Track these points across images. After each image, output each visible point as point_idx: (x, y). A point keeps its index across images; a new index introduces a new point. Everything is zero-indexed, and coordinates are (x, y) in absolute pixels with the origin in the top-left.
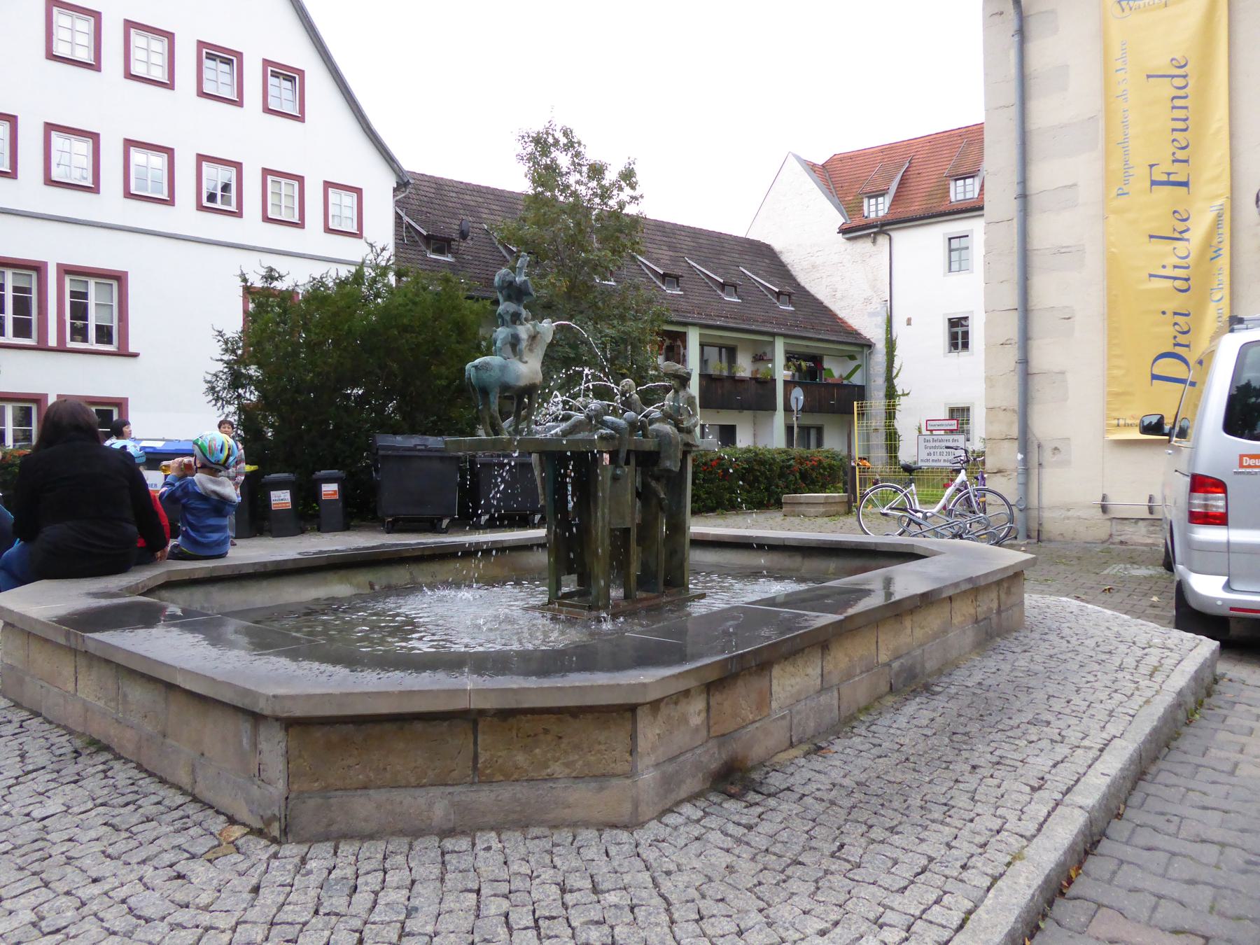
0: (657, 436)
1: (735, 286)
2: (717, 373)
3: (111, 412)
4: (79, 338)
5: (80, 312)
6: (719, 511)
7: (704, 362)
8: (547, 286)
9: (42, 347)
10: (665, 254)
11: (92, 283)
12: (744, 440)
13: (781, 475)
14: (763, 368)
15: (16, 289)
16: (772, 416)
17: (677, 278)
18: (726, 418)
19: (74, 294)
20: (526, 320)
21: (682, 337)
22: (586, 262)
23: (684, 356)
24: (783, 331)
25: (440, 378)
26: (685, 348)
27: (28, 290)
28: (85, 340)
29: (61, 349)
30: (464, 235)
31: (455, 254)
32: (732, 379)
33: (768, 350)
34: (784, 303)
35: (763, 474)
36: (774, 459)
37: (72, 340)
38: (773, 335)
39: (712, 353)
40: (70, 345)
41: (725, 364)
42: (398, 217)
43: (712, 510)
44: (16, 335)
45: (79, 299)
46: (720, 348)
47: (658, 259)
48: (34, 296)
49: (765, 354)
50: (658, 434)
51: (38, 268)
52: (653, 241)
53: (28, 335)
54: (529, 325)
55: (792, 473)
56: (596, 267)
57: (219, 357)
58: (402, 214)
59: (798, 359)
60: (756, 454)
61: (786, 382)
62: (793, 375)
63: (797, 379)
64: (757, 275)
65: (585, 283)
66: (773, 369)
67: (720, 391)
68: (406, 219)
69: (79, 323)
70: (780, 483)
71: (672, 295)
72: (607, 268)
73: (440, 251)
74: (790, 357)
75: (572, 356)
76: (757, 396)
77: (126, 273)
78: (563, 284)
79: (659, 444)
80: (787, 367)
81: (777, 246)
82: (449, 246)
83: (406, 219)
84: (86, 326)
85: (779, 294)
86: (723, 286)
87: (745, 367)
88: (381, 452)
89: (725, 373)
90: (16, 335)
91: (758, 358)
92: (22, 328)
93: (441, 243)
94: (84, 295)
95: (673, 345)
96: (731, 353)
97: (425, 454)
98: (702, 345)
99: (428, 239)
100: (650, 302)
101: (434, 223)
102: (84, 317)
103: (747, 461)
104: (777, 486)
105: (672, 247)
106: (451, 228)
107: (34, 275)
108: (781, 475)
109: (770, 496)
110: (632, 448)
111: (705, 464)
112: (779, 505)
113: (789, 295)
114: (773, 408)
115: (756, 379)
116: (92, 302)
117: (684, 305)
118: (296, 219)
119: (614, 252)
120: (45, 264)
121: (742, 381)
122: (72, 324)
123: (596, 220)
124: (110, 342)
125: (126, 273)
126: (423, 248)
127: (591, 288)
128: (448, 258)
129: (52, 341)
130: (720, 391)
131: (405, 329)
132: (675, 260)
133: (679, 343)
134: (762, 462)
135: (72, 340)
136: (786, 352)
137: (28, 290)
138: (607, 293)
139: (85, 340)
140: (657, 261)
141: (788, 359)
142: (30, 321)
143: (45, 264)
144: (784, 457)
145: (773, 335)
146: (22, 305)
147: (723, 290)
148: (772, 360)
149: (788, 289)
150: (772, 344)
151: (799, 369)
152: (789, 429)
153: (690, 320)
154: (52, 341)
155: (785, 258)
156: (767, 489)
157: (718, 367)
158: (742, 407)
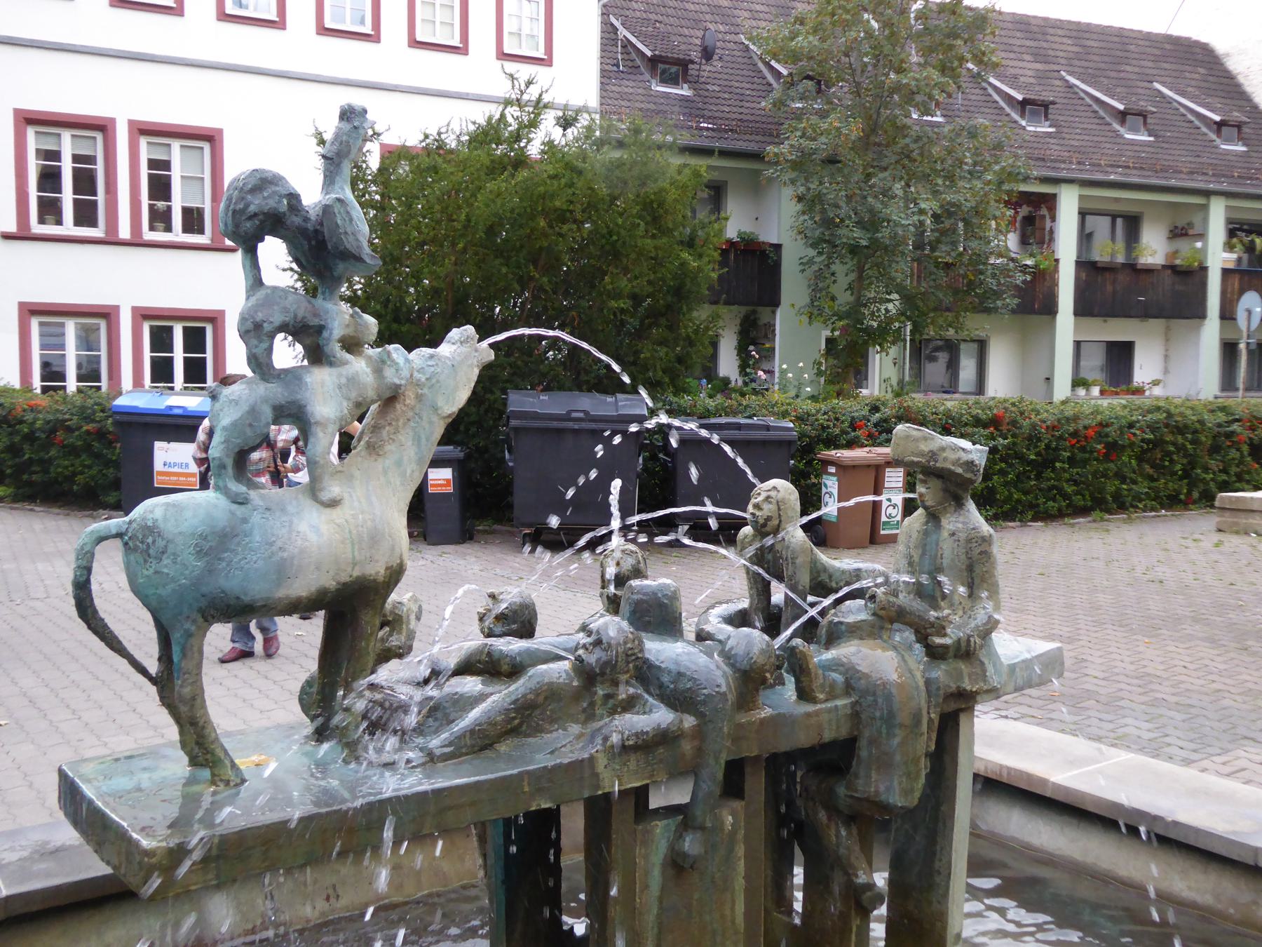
0: (849, 688)
1: (1143, 115)
2: (1106, 259)
3: (204, 329)
4: (161, 225)
5: (161, 188)
6: (1097, 514)
7: (1085, 238)
8: (828, 132)
9: (111, 240)
10: (1028, 69)
11: (176, 145)
12: (1145, 369)
13: (1215, 449)
14: (1186, 251)
15: (76, 158)
16: (1198, 329)
17: (1045, 106)
18: (1117, 330)
19: (153, 164)
20: (352, 345)
21: (1049, 202)
22: (897, 88)
23: (1052, 232)
24: (1225, 187)
25: (617, 295)
26: (1053, 219)
27: (91, 159)
28: (168, 229)
29: (137, 242)
30: (708, 54)
31: (694, 83)
32: (1132, 268)
33: (1197, 219)
34: (1228, 140)
35: (1180, 448)
36: (1201, 422)
37: (152, 228)
38: (1207, 194)
39: (1101, 226)
40: (149, 236)
41: (1120, 245)
42: (609, 33)
43: (1083, 511)
44: (78, 223)
45: (160, 165)
46: (1114, 217)
47: (1015, 77)
48: (100, 168)
49: (1190, 225)
50: (853, 682)
51: (103, 127)
52: (1009, 48)
53: (93, 223)
54: (359, 366)
55: (1236, 446)
56: (910, 96)
57: (287, 265)
58: (617, 24)
59: (1249, 232)
60: (1170, 415)
61: (1226, 272)
62: (1239, 260)
63: (1244, 266)
64: (1183, 94)
65: (892, 120)
66: (1204, 250)
67: (1109, 288)
68: (623, 32)
69: (161, 204)
70: (1213, 464)
71: (1036, 135)
72: (931, 97)
73: (673, 81)
74: (1235, 230)
75: (864, 243)
76: (1176, 295)
77: (220, 131)
78: (855, 130)
79: (855, 715)
80: (1229, 247)
81: (1220, 45)
82: (686, 70)
83: (623, 32)
84: (169, 209)
85: (1220, 125)
86: (1122, 116)
87: (1154, 248)
88: (513, 423)
89: (1120, 259)
90: (78, 223)
91: (1178, 233)
92: (85, 215)
93: (670, 67)
94: (166, 165)
95: (1034, 215)
96: (1133, 224)
97: (584, 425)
98: (1083, 214)
99: (654, 62)
100: (998, 146)
101: (665, 37)
102: (167, 196)
103: (1153, 427)
104: (1206, 469)
105: (1039, 56)
106: (688, 44)
107: (99, 137)
108: (1215, 449)
109: (1191, 486)
110: (751, 750)
111: (1075, 434)
112: (1207, 500)
113: (1239, 126)
114: (1201, 314)
115: (1173, 268)
116: (176, 174)
117: (1055, 150)
118: (456, 42)
119: (943, 69)
120: (113, 121)
121: (1149, 271)
122: (151, 207)
123: (917, 19)
124: (201, 231)
125: (220, 131)
126: (647, 76)
127: (902, 130)
128: (685, 91)
129: (125, 232)
130: (1109, 288)
131: (562, 217)
132: (1042, 77)
133: (1044, 211)
134: (1181, 429)
135: (152, 228)
136: (1229, 221)
137: (91, 159)
138: (926, 138)
139: (168, 229)
140: (1013, 81)
141: (1231, 233)
142: (95, 203)
143: (113, 121)
144: (1222, 417)
145: (1207, 194)
146: (84, 181)
147: (1123, 122)
148: (1202, 236)
149: (1237, 116)
150: (1205, 208)
151: (1250, 248)
152: (1229, 350)
153: (1064, 174)
154: (125, 232)
155: (1233, 65)
156: (1186, 474)
157: (1108, 250)
158: (1146, 313)
